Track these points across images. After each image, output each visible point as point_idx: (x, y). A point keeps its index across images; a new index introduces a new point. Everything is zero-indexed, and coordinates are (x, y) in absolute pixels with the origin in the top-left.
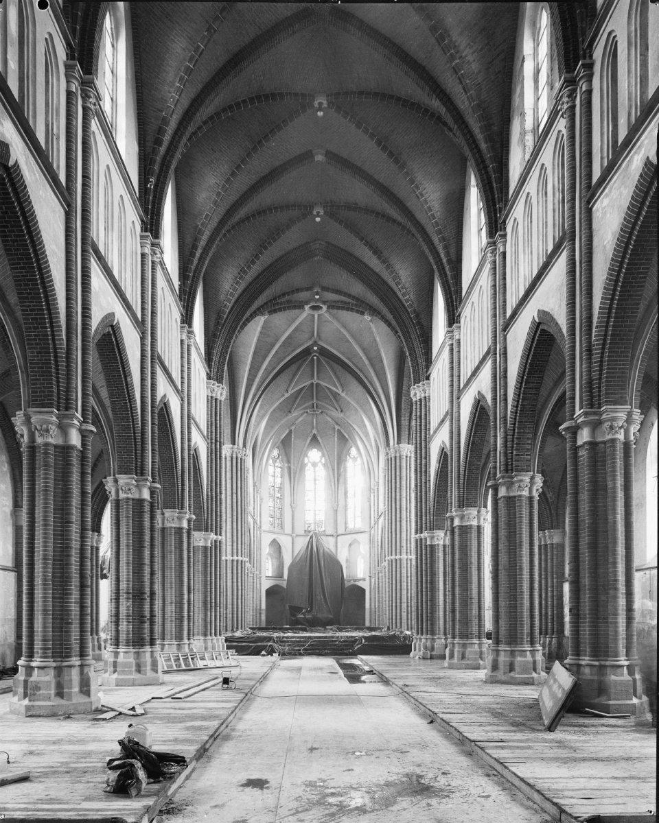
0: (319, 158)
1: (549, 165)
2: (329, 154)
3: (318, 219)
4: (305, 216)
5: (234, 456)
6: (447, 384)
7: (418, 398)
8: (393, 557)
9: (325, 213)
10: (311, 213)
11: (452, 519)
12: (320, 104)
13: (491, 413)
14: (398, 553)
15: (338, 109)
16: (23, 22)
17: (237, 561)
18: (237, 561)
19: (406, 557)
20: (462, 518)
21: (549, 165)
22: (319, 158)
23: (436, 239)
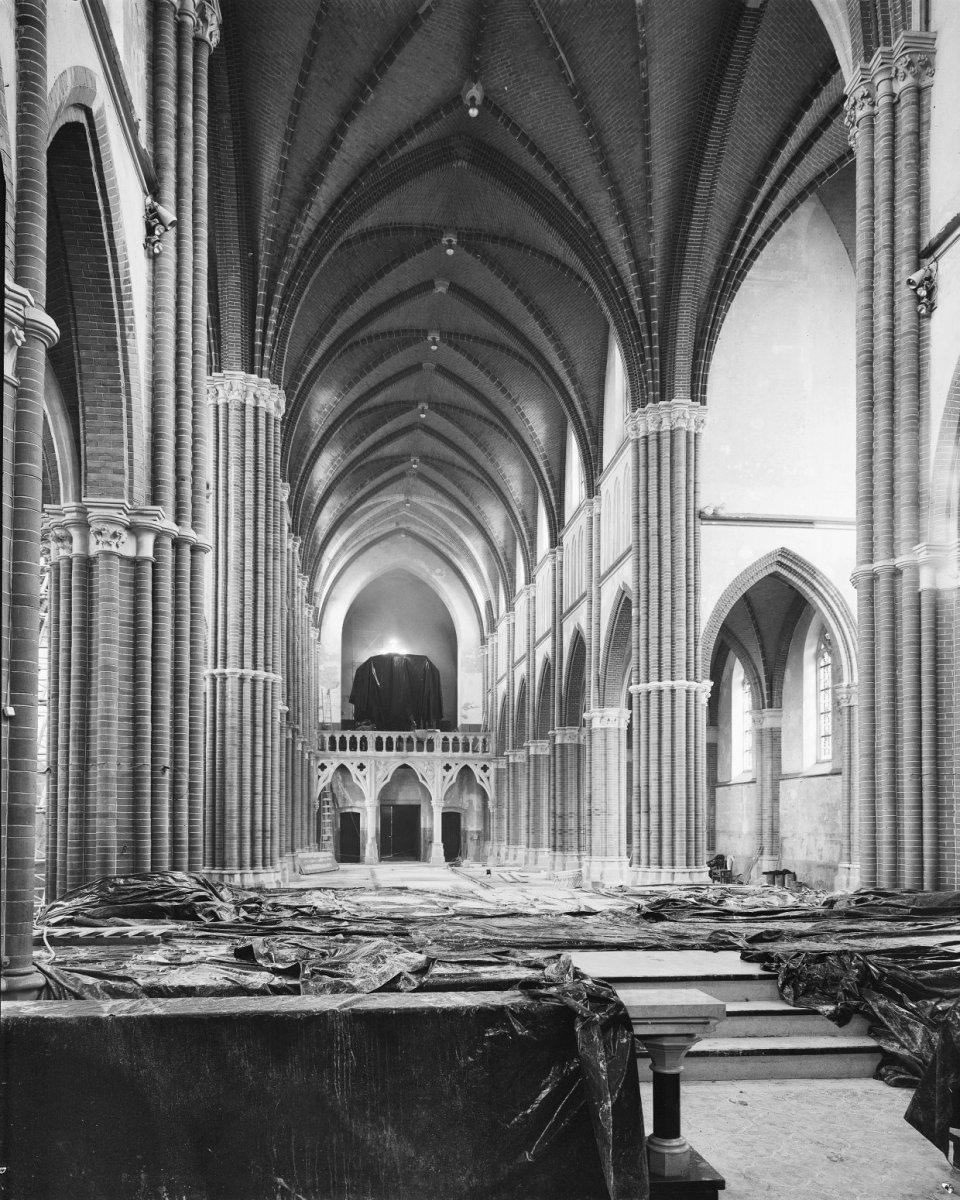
0: (441, 288)
1: (621, 479)
2: (455, 288)
3: (473, 112)
4: (428, 244)
5: (250, 401)
6: (551, 592)
7: (642, 434)
8: (654, 685)
9: (458, 243)
10: (440, 241)
11: (528, 748)
12: (434, 339)
13: (587, 641)
14: (666, 673)
15: (468, 249)
16: (114, 77)
17: (254, 681)
18: (254, 681)
19: (677, 684)
20: (515, 756)
21: (621, 479)
22: (441, 288)
23: (541, 463)
